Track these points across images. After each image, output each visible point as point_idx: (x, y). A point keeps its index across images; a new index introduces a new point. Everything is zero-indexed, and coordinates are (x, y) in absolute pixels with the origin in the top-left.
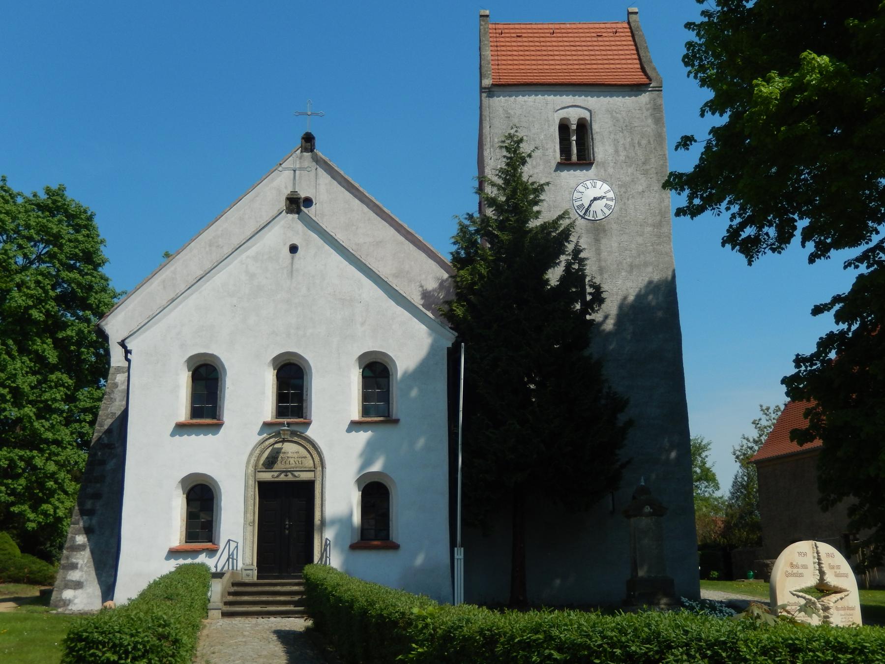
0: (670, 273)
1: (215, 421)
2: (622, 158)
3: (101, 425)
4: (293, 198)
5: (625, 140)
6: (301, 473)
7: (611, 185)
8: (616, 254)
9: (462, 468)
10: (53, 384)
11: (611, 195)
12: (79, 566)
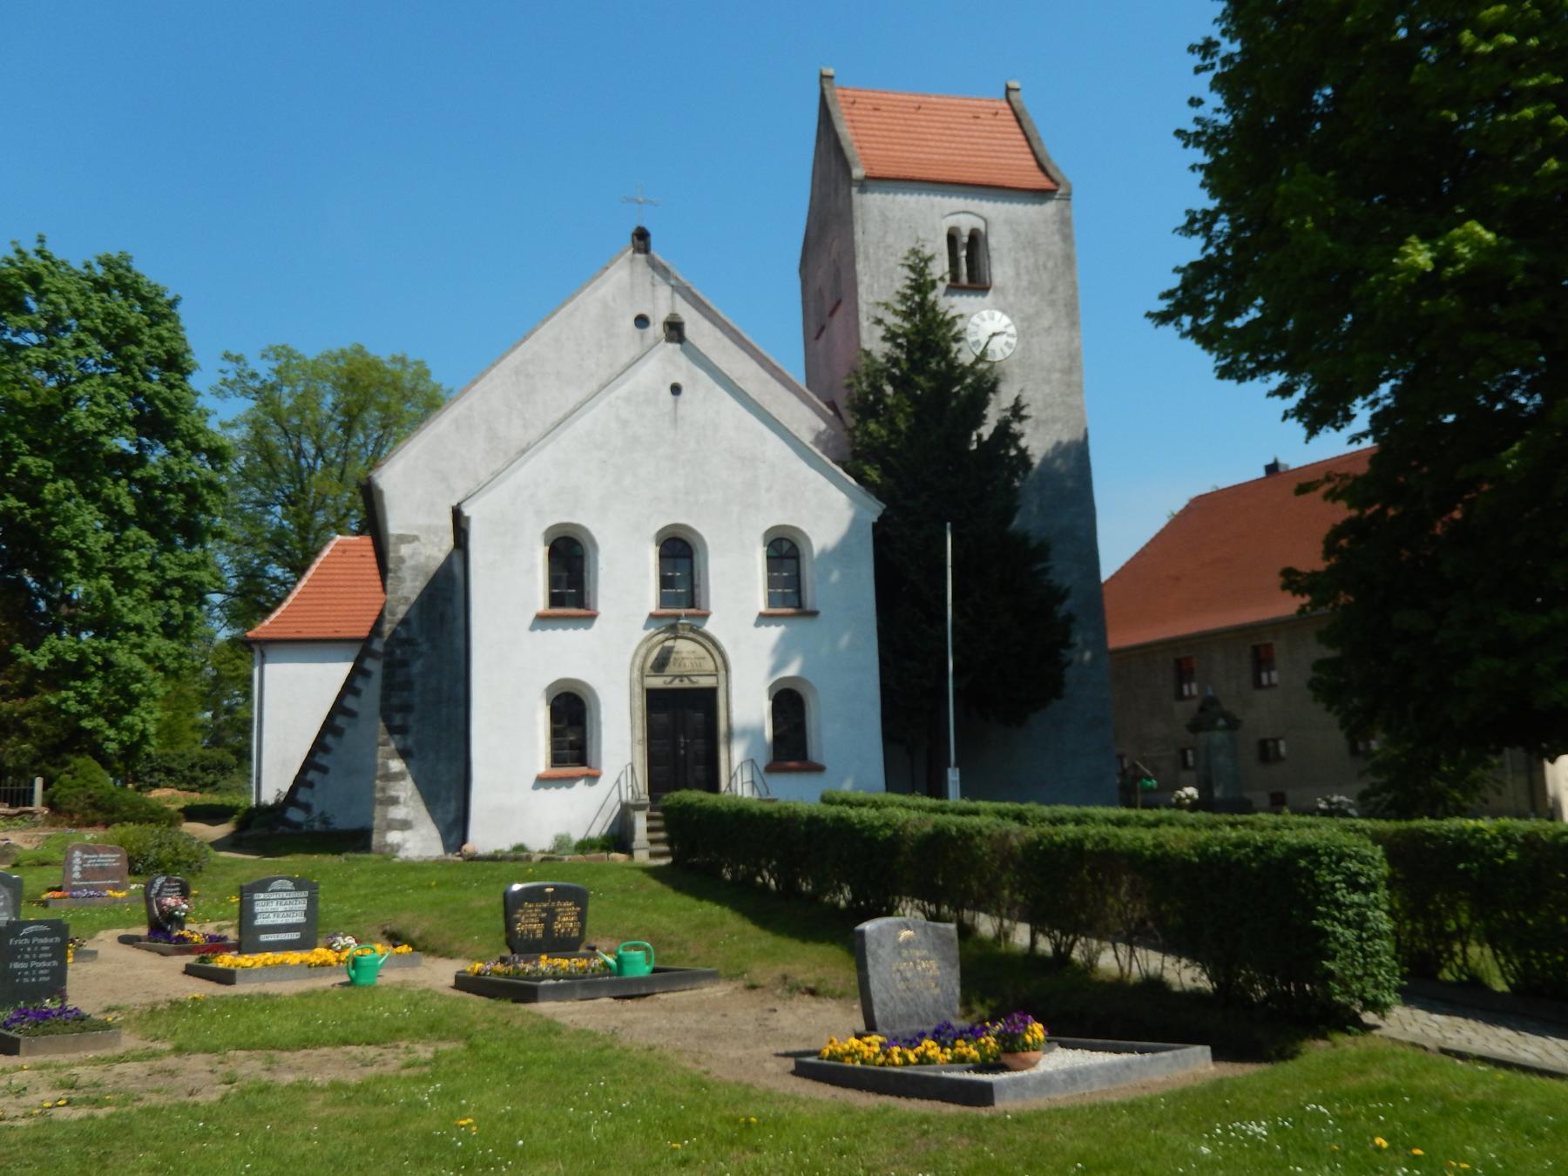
0: (1082, 432)
1: (582, 612)
2: (1024, 283)
3: (393, 614)
7: (1011, 317)
10: (131, 545)
11: (1012, 330)
12: (402, 800)
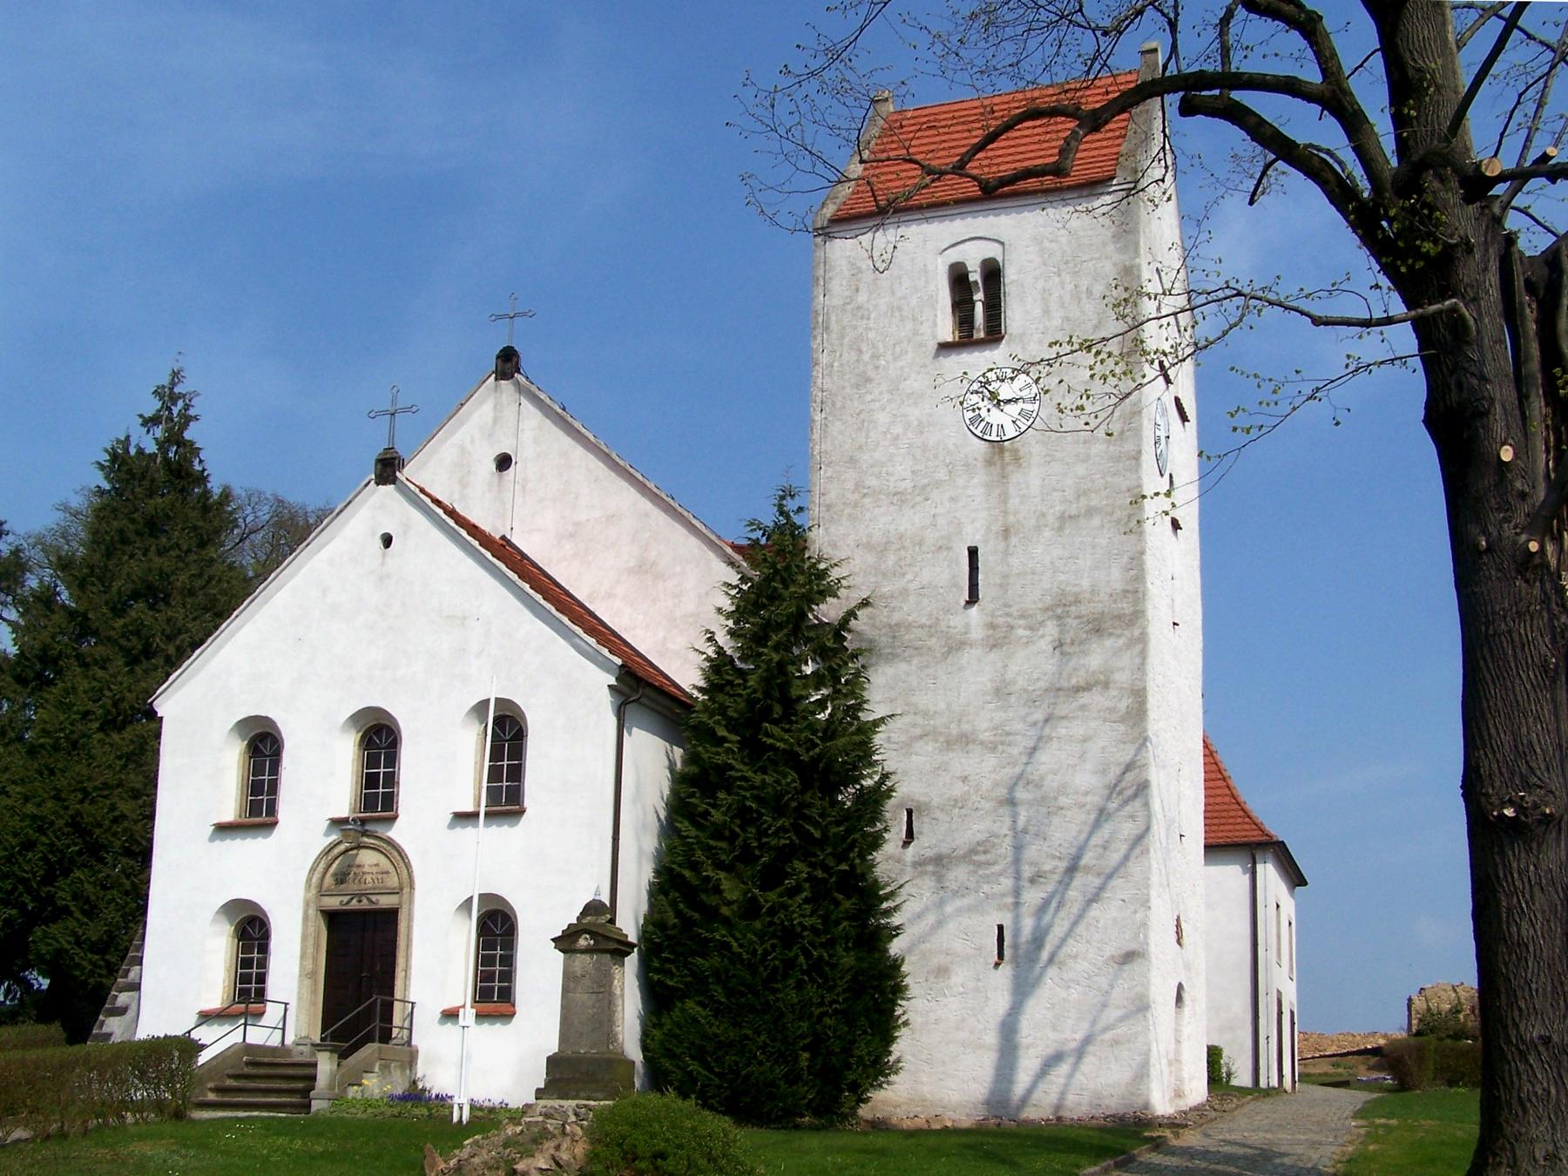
4: (385, 459)
5: (1063, 288)
6: (378, 897)
8: (1036, 500)
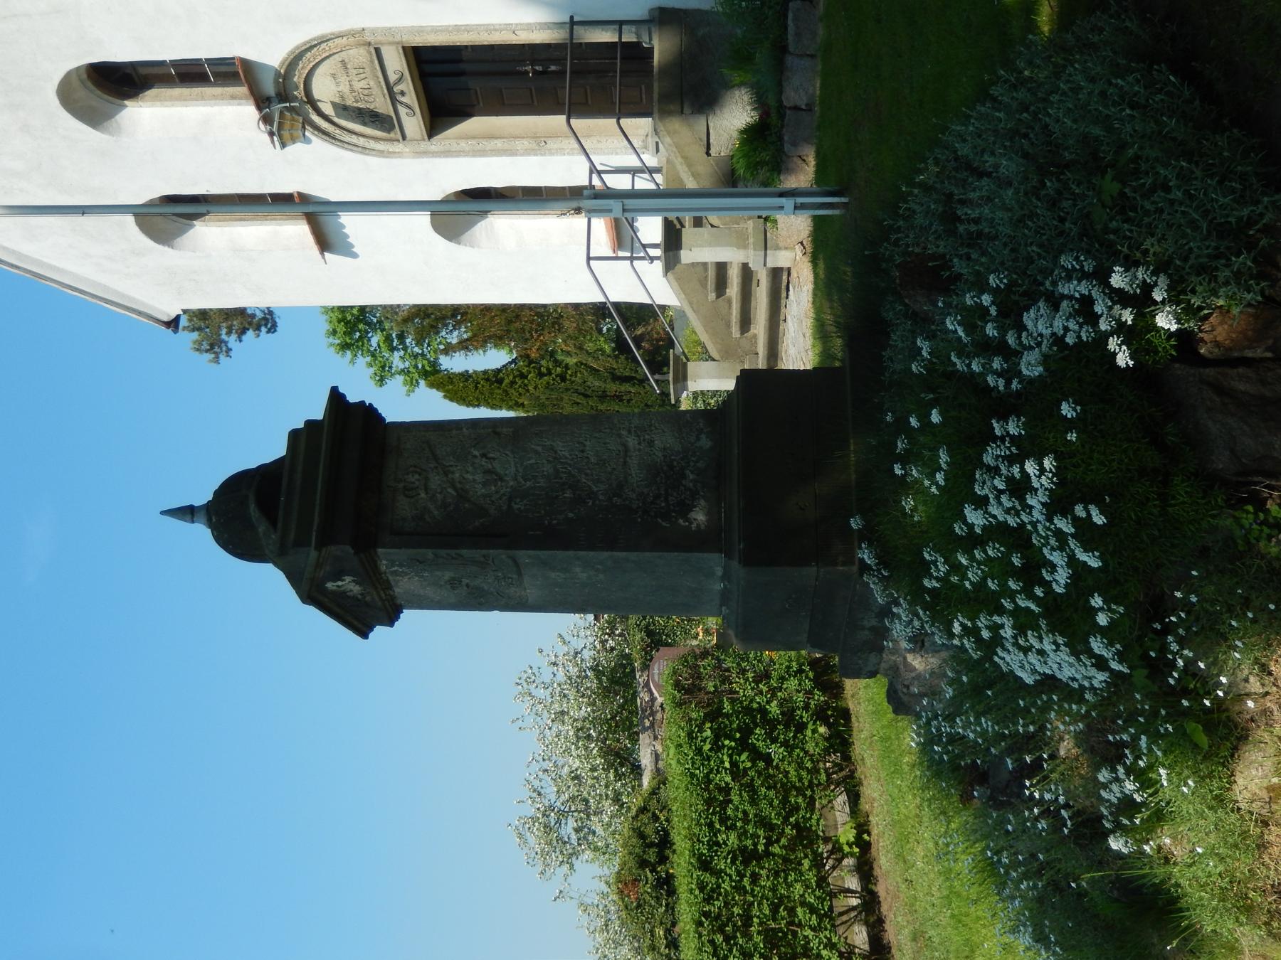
9: (493, 407)
